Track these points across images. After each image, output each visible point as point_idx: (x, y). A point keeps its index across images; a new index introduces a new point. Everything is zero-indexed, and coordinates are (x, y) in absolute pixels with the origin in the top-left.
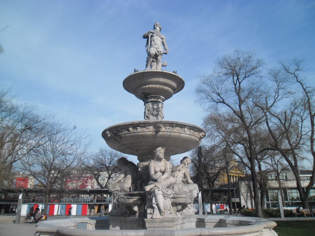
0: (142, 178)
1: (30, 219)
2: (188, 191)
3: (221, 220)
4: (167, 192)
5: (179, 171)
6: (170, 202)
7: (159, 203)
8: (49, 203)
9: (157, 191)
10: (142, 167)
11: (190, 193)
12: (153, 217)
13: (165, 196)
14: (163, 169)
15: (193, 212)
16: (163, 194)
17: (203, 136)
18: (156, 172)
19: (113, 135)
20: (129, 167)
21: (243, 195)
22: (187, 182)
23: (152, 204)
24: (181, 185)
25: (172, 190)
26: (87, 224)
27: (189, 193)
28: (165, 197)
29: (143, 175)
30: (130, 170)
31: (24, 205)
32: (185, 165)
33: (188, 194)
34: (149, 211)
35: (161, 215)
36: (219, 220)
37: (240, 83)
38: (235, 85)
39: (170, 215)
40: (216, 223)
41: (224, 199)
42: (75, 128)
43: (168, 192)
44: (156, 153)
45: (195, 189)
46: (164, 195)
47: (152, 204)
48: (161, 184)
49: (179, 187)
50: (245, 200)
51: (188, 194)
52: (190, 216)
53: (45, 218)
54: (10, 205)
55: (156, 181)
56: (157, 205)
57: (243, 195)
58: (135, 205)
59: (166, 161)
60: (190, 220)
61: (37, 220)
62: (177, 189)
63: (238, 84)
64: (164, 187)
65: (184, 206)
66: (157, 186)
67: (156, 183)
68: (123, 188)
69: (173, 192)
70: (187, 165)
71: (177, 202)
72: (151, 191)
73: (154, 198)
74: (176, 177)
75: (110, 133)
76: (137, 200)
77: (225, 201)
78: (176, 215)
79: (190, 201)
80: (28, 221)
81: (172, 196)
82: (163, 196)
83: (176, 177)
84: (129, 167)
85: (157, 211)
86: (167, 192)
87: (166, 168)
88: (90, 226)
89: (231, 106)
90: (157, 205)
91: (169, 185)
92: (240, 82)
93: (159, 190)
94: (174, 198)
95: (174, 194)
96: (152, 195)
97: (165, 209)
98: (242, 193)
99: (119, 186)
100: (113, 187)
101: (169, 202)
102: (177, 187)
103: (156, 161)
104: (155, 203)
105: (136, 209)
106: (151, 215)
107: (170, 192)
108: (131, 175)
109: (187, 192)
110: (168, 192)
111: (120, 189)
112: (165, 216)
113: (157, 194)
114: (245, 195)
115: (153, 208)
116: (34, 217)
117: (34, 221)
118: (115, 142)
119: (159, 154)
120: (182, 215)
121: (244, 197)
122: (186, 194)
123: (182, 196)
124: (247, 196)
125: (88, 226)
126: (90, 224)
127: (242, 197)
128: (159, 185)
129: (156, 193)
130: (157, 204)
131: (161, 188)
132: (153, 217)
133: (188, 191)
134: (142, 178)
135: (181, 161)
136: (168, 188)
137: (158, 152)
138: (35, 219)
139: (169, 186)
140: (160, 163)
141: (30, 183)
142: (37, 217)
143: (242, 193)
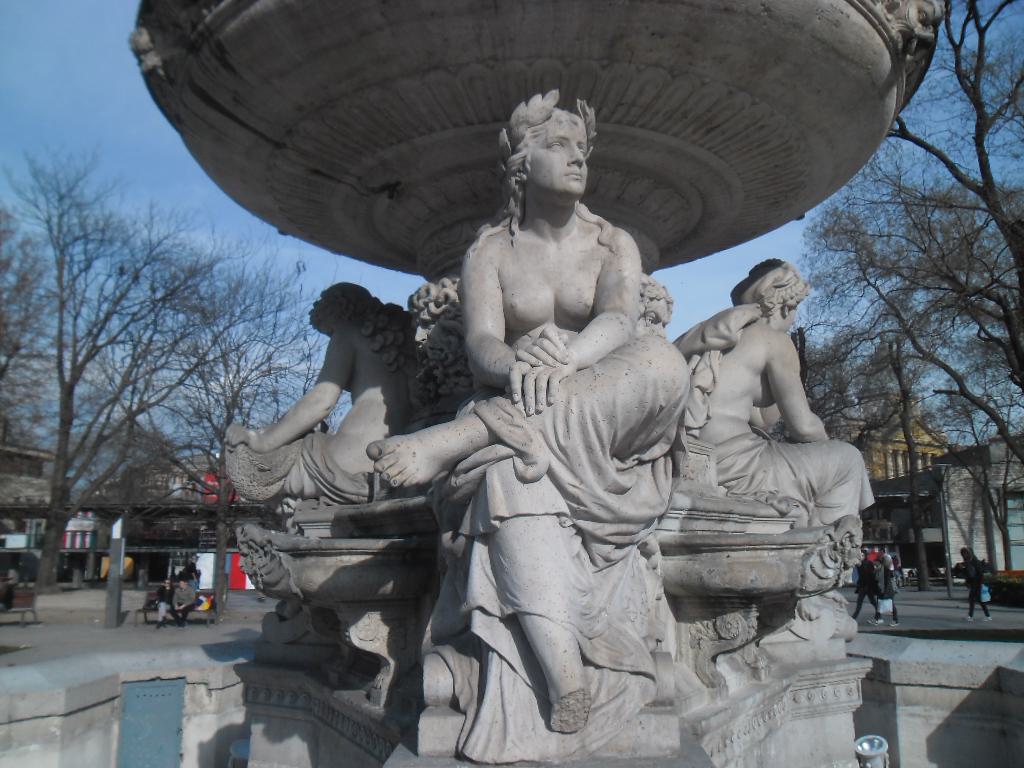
0: (438, 396)
1: (156, 609)
2: (795, 494)
3: (1000, 673)
4: (612, 500)
5: (726, 350)
6: (654, 589)
7: (526, 603)
8: (229, 550)
9: (503, 492)
10: (435, 317)
11: (811, 505)
12: (467, 753)
13: (594, 533)
14: (582, 291)
15: (834, 637)
16: (575, 514)
17: (924, 22)
18: (516, 328)
19: (177, 52)
20: (372, 336)
21: (955, 518)
22: (786, 434)
23: (468, 617)
24: (744, 455)
25: (666, 482)
26: (188, 687)
27: (805, 506)
28: (600, 549)
29: (446, 376)
30: (380, 351)
31: (205, 555)
32: (766, 312)
33: (794, 512)
34: (440, 677)
35: (549, 727)
36: (990, 672)
37: (982, 32)
38: (957, 48)
39: (653, 722)
40: (966, 693)
41: (883, 533)
42: (302, 269)
43: (621, 491)
44: (515, 151)
45: (841, 479)
46: (582, 523)
47: (464, 608)
48: (547, 412)
49: (728, 462)
50: (964, 536)
51: (794, 512)
52: (818, 669)
53: (211, 608)
54: (166, 556)
55: (499, 388)
56: (515, 621)
57: (955, 518)
58: (362, 605)
59: (609, 227)
60: (817, 700)
61: (180, 615)
62: (712, 476)
63: (972, 41)
64: (576, 443)
65: (775, 608)
66: (503, 430)
67: (495, 412)
68: (330, 479)
69: (684, 502)
70: (777, 313)
71: (717, 581)
72: (455, 490)
73: (480, 551)
74: (703, 390)
75: (153, 41)
76: (362, 565)
77: (886, 538)
78: (712, 685)
79: (831, 573)
80: (151, 616)
81: (671, 530)
82: (580, 531)
83: (703, 390)
84: (372, 336)
85: (509, 685)
86: (612, 500)
87: (612, 279)
88: (206, 700)
89: (938, 148)
90: (515, 621)
91: (636, 417)
92: (983, 24)
93: (530, 472)
94: (687, 547)
95: (693, 514)
96: (465, 529)
97: (600, 658)
98: (952, 512)
99: (306, 465)
100: (262, 470)
101: (637, 587)
102: (712, 464)
103: (515, 227)
104: (492, 603)
105: (369, 633)
106: (457, 720)
107: (644, 490)
108: (384, 392)
109: (787, 499)
110: (621, 491)
111: (309, 489)
112: (598, 735)
113: (503, 512)
114: (963, 516)
115: (478, 650)
116: (170, 602)
117: (170, 617)
118: (213, 115)
119: (542, 152)
120: (755, 671)
121: (959, 524)
122: (783, 514)
123: (755, 528)
124: (972, 520)
125: (193, 700)
126: (202, 689)
127: (951, 524)
128: (531, 426)
129: (499, 505)
130: (509, 611)
131: (544, 456)
132: (475, 751)
133: (795, 494)
134: (438, 396)
135: (738, 295)
136: (621, 452)
137: (528, 134)
138: (172, 611)
139: (632, 434)
140: (551, 247)
141: (245, 483)
142: (180, 605)
143: (952, 512)
